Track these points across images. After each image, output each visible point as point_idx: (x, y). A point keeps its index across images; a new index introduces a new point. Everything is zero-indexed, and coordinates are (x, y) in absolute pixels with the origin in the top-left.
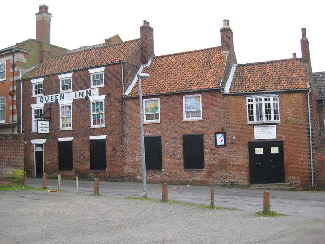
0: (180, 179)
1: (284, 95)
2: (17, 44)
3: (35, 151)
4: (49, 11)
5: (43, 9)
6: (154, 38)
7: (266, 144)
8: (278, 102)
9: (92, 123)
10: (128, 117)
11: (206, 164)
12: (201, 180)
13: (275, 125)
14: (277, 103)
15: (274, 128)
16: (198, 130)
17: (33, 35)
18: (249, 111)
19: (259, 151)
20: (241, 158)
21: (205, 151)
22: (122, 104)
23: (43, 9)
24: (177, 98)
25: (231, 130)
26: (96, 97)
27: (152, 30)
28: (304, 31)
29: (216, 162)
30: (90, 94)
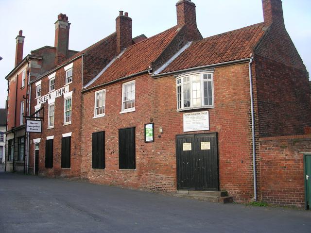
0: (117, 180)
1: (220, 70)
2: (32, 52)
3: (35, 149)
4: (70, 21)
5: (63, 18)
6: (176, 15)
7: (196, 137)
8: (212, 80)
9: (65, 120)
10: (84, 113)
11: (137, 163)
12: (134, 182)
13: (208, 112)
14: (210, 83)
15: (205, 115)
16: (132, 123)
17: (52, 43)
18: (210, 95)
19: (187, 147)
20: (169, 159)
21: (137, 147)
22: (82, 98)
23: (63, 18)
24: (117, 86)
25: (159, 121)
26: (68, 95)
27: (130, 20)
28: (21, 32)
29: (145, 161)
30: (64, 92)
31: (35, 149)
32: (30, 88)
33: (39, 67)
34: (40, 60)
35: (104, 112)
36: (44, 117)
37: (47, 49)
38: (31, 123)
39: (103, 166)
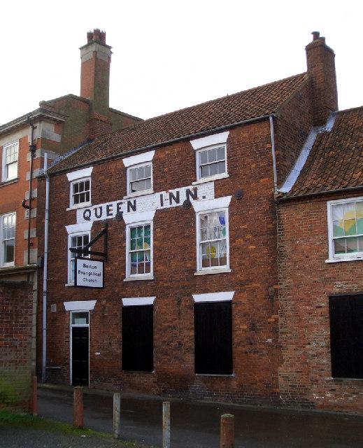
3: (72, 325)
5: (97, 38)
10: (288, 248)
22: (274, 216)
23: (97, 38)
26: (210, 203)
30: (195, 197)
31: (72, 325)
32: (47, 183)
33: (56, 138)
34: (60, 122)
35: (88, 200)
36: (110, 252)
37: (70, 98)
38: (85, 266)
39: (228, 368)
